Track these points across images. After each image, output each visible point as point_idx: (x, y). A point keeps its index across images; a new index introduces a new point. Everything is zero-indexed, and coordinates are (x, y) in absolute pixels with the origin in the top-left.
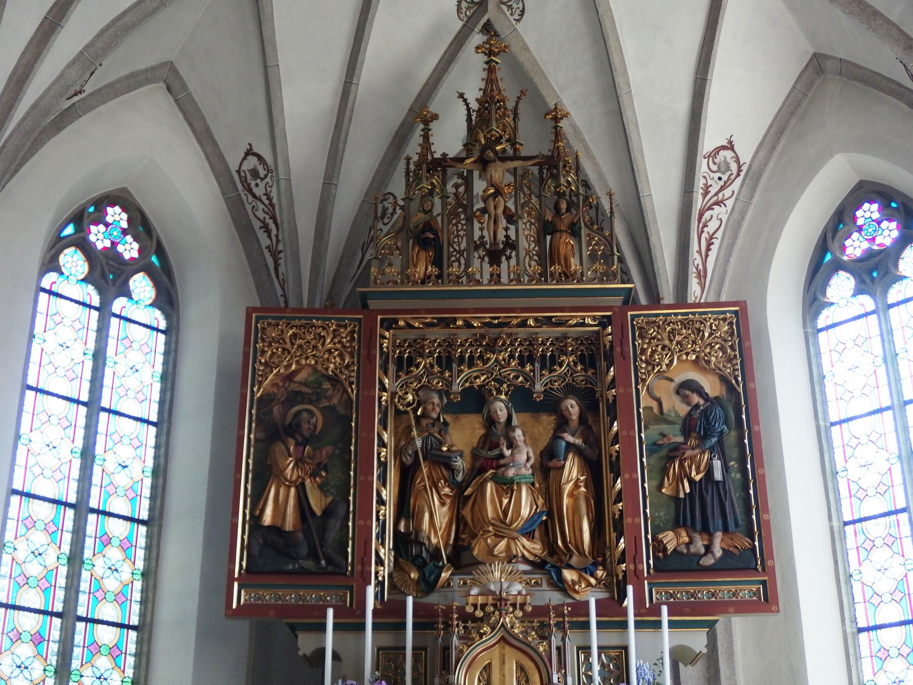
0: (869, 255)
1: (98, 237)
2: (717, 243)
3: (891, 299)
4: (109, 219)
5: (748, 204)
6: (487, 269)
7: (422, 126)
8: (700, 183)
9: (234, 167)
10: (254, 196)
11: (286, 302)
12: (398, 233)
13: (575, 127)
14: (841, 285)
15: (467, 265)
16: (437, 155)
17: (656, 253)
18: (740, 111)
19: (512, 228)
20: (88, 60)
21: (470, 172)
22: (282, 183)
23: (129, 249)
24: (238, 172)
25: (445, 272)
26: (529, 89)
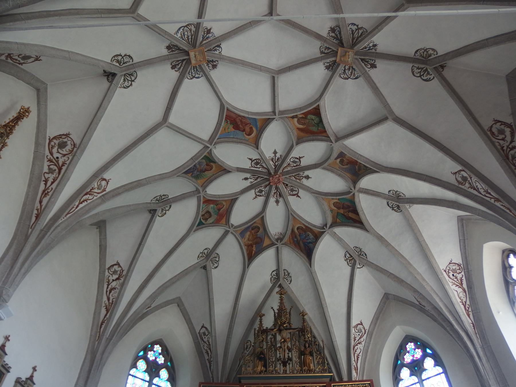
0: (413, 361)
1: (151, 356)
2: (360, 357)
3: (423, 377)
4: (155, 349)
5: (369, 343)
6: (282, 368)
7: (259, 318)
8: (352, 336)
9: (197, 331)
10: (204, 341)
11: (213, 379)
12: (252, 355)
13: (310, 318)
14: (405, 373)
15: (275, 367)
16: (265, 328)
17: (340, 361)
18: (363, 312)
19: (290, 353)
20: (153, 297)
21: (276, 334)
22: (213, 337)
23: (161, 360)
24: (199, 333)
25: (268, 369)
26: (294, 305)
